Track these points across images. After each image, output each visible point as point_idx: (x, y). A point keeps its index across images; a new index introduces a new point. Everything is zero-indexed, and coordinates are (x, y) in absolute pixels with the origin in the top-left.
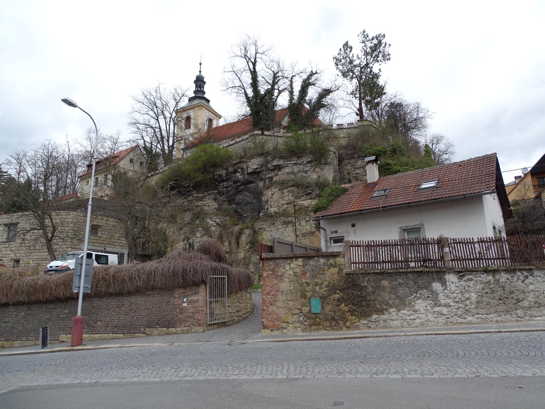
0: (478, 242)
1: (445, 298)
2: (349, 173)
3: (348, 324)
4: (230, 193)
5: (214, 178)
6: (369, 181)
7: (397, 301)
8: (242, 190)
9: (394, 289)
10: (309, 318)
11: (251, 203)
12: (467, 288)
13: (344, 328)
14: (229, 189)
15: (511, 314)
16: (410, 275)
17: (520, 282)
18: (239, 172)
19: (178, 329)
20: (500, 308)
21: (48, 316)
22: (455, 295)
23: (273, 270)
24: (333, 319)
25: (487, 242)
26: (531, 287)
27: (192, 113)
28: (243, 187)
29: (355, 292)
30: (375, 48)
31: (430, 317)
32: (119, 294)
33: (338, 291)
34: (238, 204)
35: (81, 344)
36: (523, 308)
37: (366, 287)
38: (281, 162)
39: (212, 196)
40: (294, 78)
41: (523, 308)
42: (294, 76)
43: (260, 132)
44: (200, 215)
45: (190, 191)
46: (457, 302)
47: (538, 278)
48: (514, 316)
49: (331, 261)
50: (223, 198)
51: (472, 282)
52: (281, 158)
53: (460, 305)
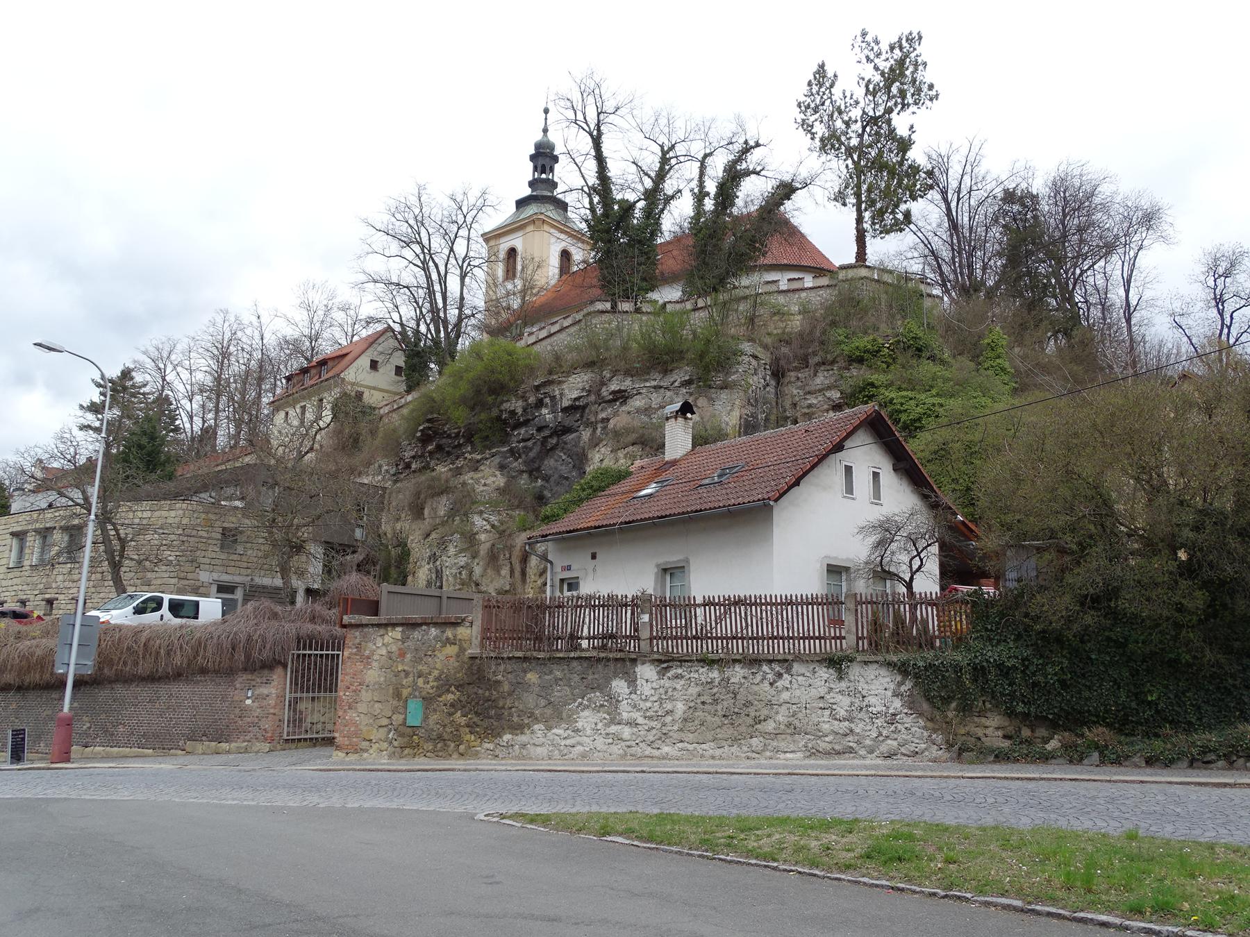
0: (705, 605)
1: (630, 709)
2: (795, 405)
3: (462, 747)
4: (532, 455)
5: (499, 418)
7: (549, 711)
8: (553, 449)
9: (545, 688)
10: (402, 735)
11: (567, 478)
12: (670, 693)
13: (455, 755)
14: (530, 444)
15: (740, 745)
16: (575, 664)
17: (766, 684)
18: (546, 406)
19: (233, 745)
20: (721, 734)
21: (50, 712)
22: (649, 704)
23: (359, 646)
24: (440, 737)
25: (718, 604)
26: (785, 696)
27: (517, 241)
28: (554, 441)
29: (480, 691)
30: (895, 74)
31: (600, 743)
32: (152, 678)
33: (453, 688)
34: (546, 479)
35: (68, 760)
36: (765, 734)
37: (498, 682)
38: (627, 384)
39: (497, 460)
40: (709, 161)
41: (765, 734)
42: (711, 154)
43: (608, 306)
44: (464, 505)
45: (460, 446)
46: (650, 718)
47: (800, 678)
48: (745, 749)
49: (449, 633)
50: (517, 465)
51: (682, 682)
52: (628, 373)
53: (653, 724)
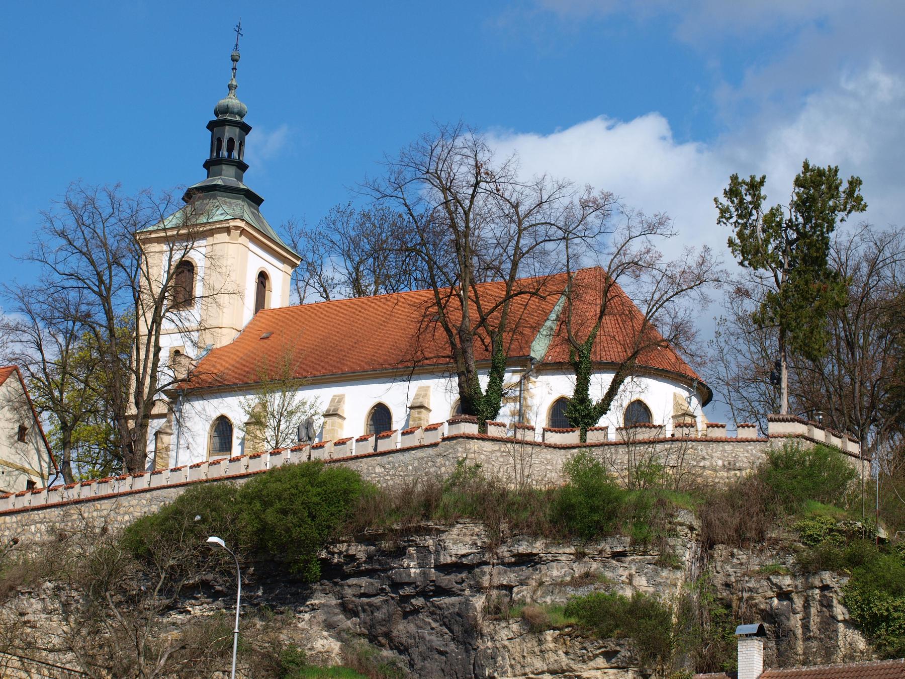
3: (141, 574)
6: (479, 529)
8: (416, 611)
18: (410, 557)
38: (538, 547)
